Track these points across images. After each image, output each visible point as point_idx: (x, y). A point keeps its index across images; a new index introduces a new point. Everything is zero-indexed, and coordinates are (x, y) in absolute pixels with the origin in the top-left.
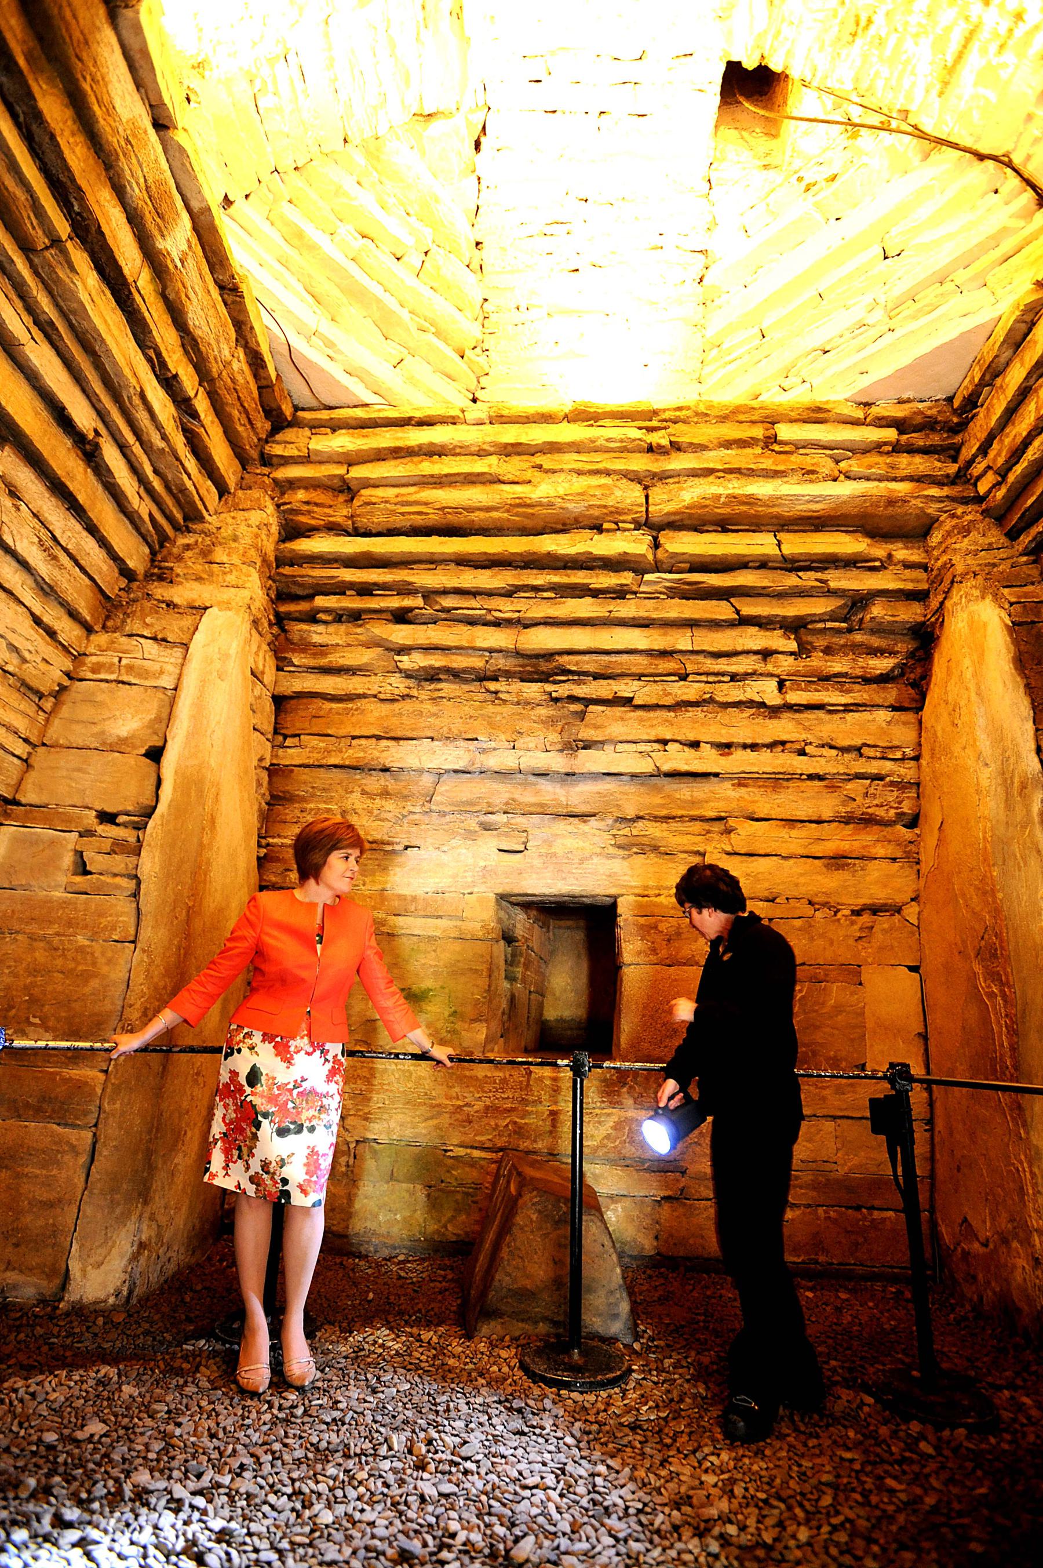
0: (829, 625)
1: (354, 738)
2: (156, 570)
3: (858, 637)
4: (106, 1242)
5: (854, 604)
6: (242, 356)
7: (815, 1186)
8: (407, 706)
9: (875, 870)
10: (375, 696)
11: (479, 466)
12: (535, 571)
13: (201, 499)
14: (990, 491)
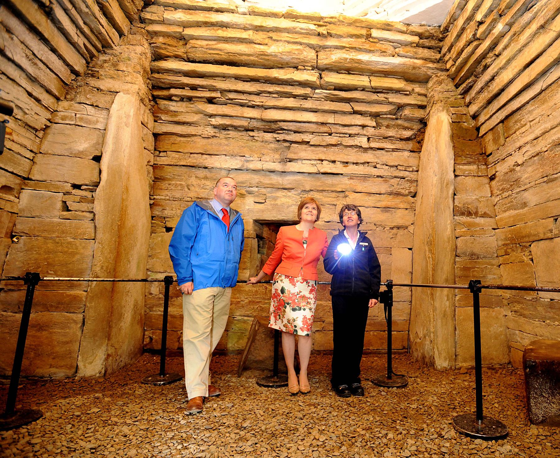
0: (389, 116)
1: (191, 153)
2: (90, 72)
3: (399, 122)
4: (93, 355)
5: (398, 109)
8: (214, 140)
9: (400, 213)
10: (200, 136)
11: (245, 35)
12: (269, 85)
13: (110, 38)
14: (450, 68)
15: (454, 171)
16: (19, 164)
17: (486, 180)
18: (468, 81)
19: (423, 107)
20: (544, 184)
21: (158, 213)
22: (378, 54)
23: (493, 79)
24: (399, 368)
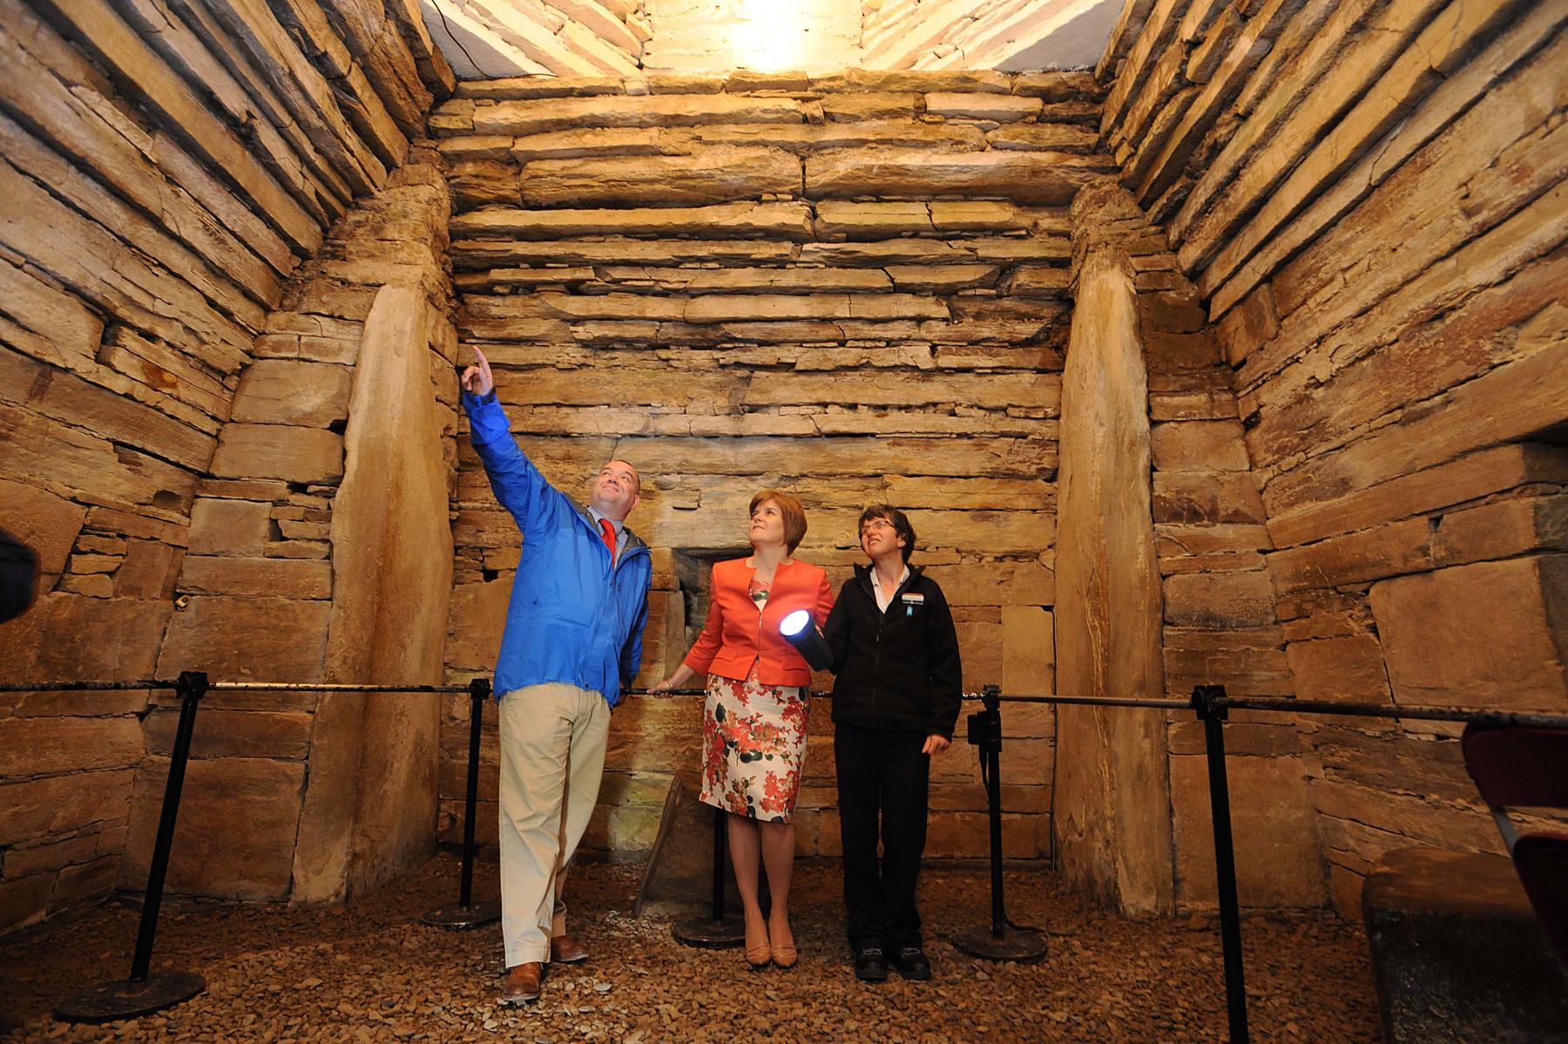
0: (979, 292)
1: (536, 406)
3: (1006, 303)
5: (1002, 272)
6: (393, 29)
7: (952, 795)
8: (584, 374)
9: (1017, 521)
11: (640, 138)
15: (1149, 411)
16: (191, 447)
17: (1234, 430)
18: (1171, 190)
19: (1062, 263)
20: (1396, 428)
21: (467, 540)
22: (945, 149)
23: (1235, 175)
24: (1024, 905)
